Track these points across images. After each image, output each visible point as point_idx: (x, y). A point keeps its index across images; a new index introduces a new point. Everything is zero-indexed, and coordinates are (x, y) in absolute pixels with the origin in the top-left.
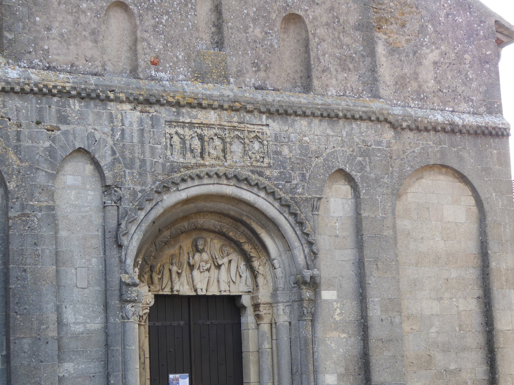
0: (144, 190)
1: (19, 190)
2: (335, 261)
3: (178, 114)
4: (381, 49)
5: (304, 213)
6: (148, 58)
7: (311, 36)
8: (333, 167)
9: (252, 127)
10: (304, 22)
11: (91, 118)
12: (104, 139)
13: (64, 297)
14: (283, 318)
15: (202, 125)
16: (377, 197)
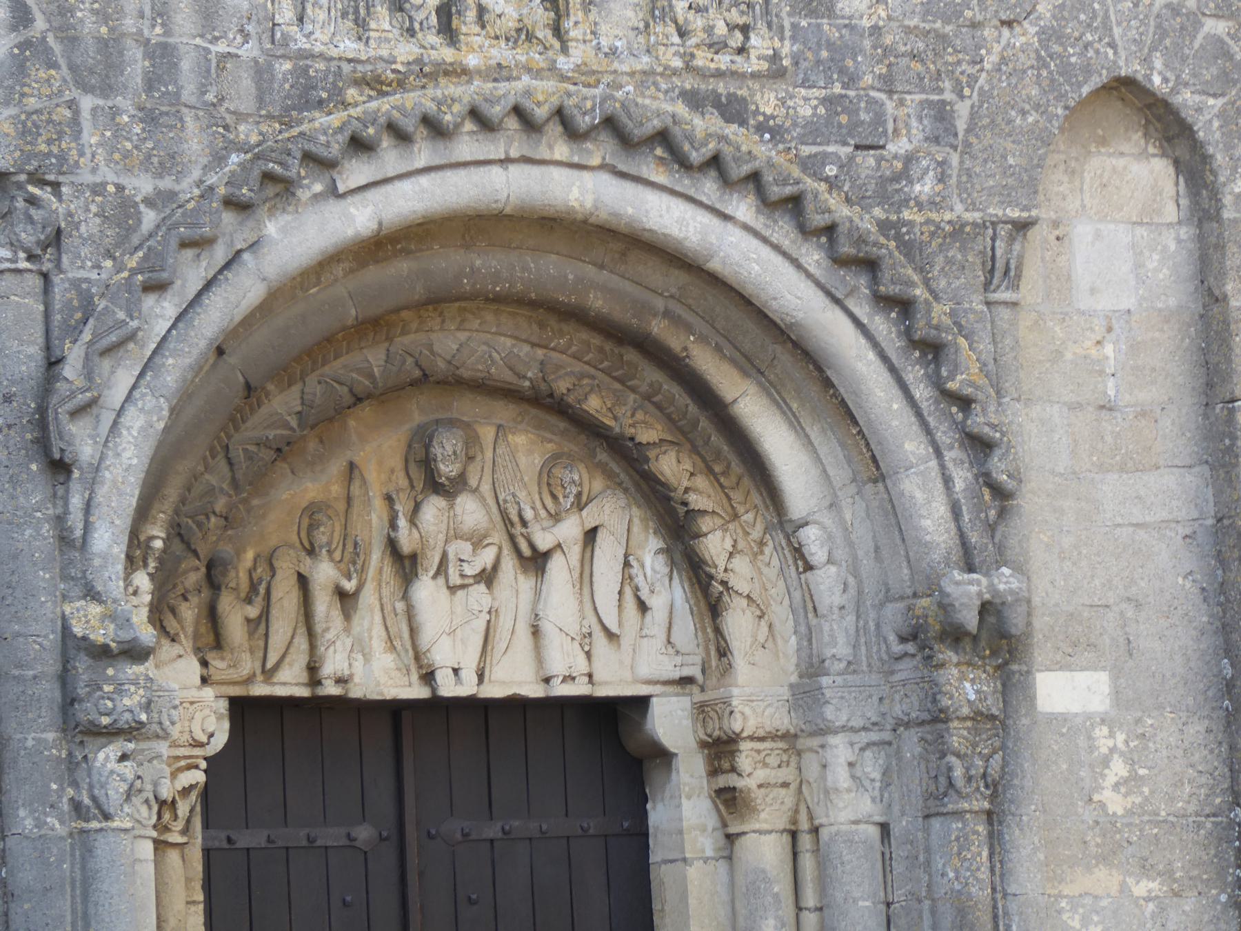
0: (171, 195)
5: (949, 295)
8: (1087, 70)
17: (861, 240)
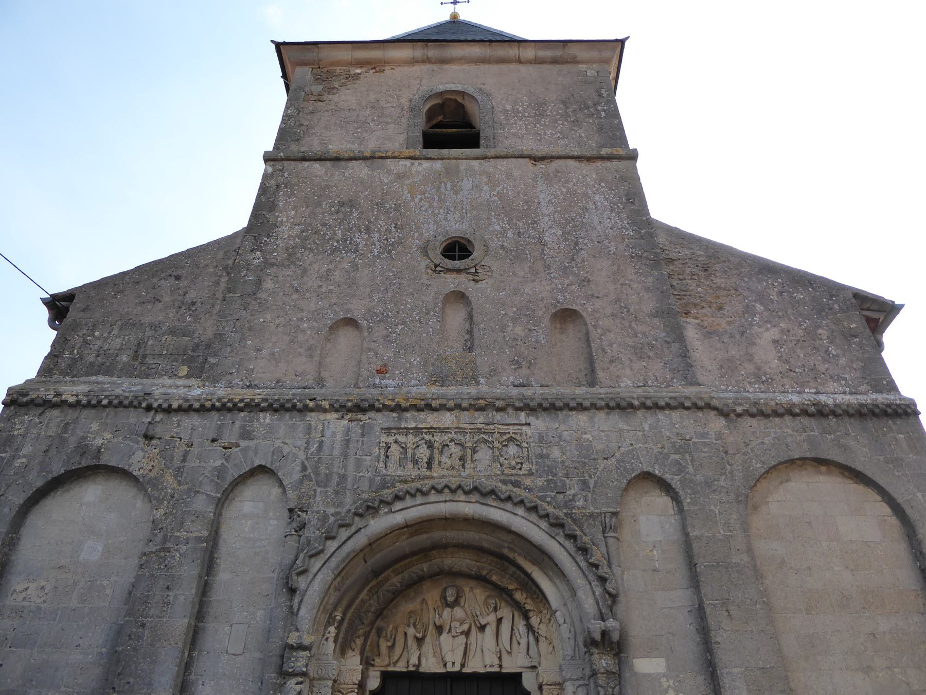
0: (339, 513)
2: (654, 607)
3: (400, 419)
4: (691, 333)
5: (591, 534)
6: (374, 367)
7: (590, 328)
9: (506, 427)
10: (581, 316)
12: (294, 454)
15: (431, 430)
16: (712, 507)
17: (557, 518)
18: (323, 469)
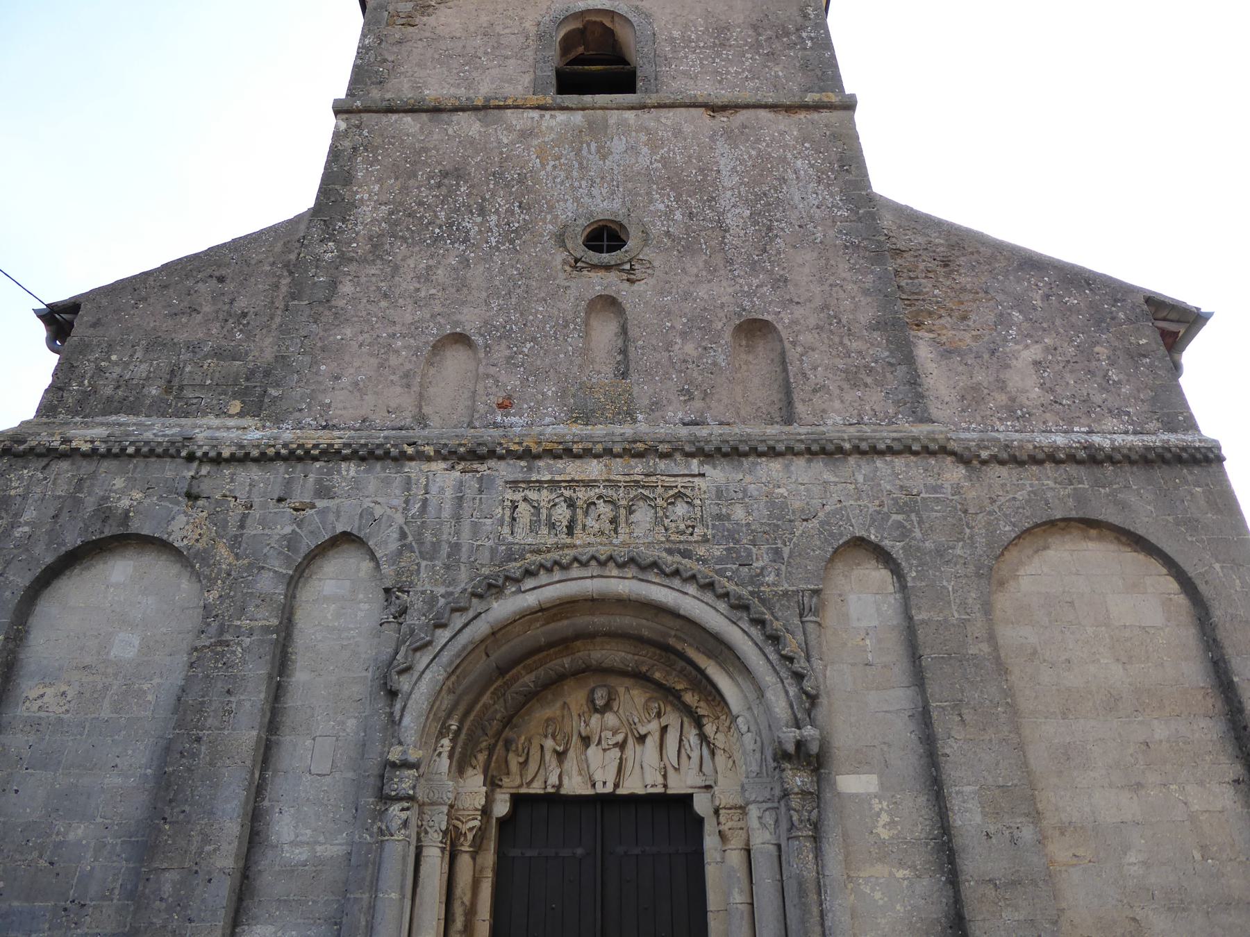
0: (452, 593)
1: (221, 603)
2: (865, 709)
3: (530, 469)
4: (924, 352)
5: (784, 618)
6: (494, 400)
7: (787, 345)
8: (841, 535)
10: (775, 328)
11: (371, 488)
13: (281, 792)
14: (762, 839)
15: (572, 483)
16: (945, 583)
18: (428, 536)
